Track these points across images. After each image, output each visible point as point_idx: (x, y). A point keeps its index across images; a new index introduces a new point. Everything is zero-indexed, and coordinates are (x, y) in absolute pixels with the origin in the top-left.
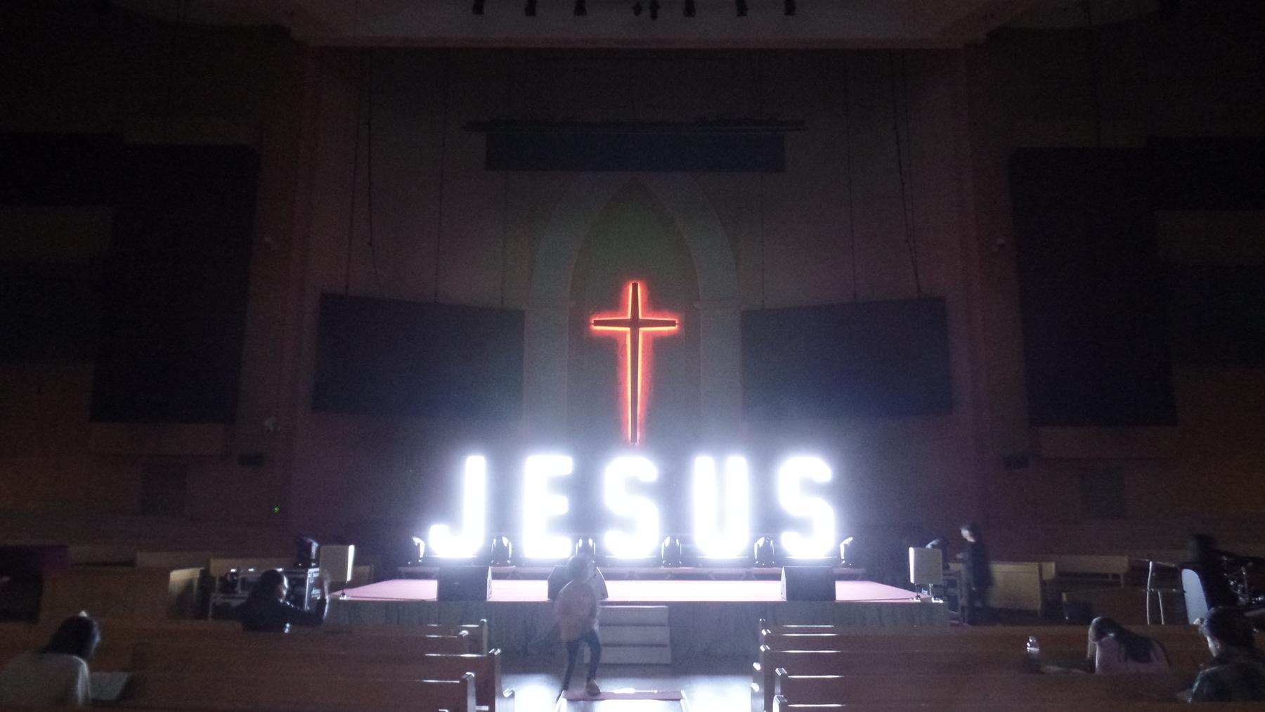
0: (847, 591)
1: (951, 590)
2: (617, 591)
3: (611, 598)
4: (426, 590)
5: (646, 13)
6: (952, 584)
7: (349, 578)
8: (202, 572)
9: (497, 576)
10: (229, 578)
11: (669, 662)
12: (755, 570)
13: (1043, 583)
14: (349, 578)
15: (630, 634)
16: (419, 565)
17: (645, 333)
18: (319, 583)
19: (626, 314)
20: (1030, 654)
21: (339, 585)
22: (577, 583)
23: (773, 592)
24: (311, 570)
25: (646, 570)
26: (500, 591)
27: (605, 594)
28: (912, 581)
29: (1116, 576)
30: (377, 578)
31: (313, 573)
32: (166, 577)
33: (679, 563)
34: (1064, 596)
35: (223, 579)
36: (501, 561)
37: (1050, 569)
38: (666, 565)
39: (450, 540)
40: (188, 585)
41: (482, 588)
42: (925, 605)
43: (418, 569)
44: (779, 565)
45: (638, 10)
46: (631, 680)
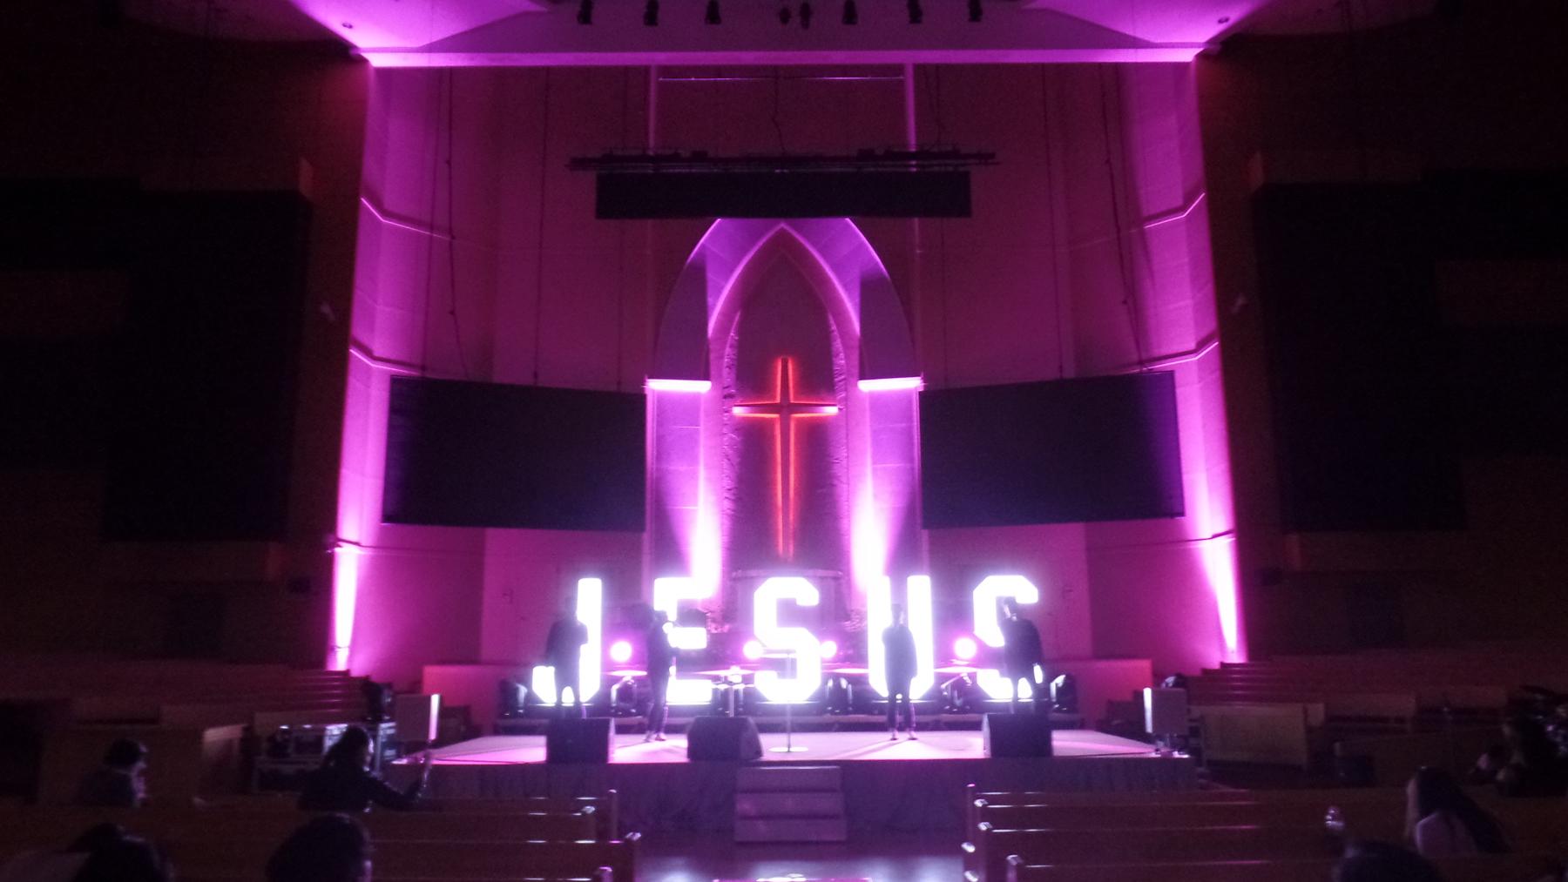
0: (1066, 743)
1: (1193, 741)
2: (774, 747)
3: (766, 757)
4: (532, 751)
5: (796, 20)
6: (1194, 732)
7: (433, 735)
8: (246, 730)
9: (622, 730)
10: (279, 738)
11: (843, 838)
12: (828, 718)
13: (1309, 730)
14: (433, 735)
15: (789, 803)
16: (517, 715)
17: (798, 420)
18: (391, 742)
19: (774, 397)
20: (1332, 829)
21: (421, 745)
22: (725, 735)
23: (974, 746)
24: (384, 726)
25: (802, 720)
26: (626, 751)
27: (759, 752)
28: (1149, 728)
29: (1401, 720)
30: (471, 731)
31: (386, 728)
32: (197, 736)
33: (847, 708)
34: (1337, 745)
35: (272, 739)
36: (640, 709)
37: (1318, 712)
38: (832, 712)
39: (585, 669)
40: (228, 744)
41: (603, 748)
42: (1166, 761)
43: (520, 721)
44: (982, 712)
45: (785, 16)
46: (797, 863)
